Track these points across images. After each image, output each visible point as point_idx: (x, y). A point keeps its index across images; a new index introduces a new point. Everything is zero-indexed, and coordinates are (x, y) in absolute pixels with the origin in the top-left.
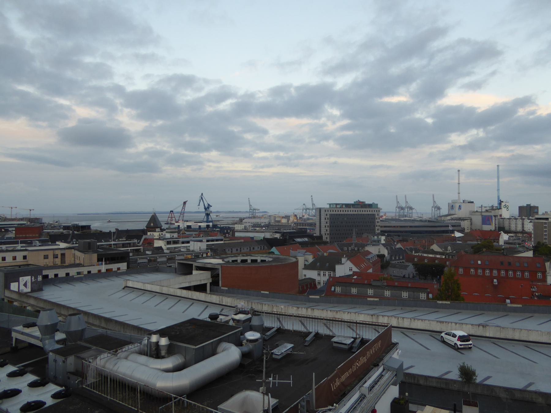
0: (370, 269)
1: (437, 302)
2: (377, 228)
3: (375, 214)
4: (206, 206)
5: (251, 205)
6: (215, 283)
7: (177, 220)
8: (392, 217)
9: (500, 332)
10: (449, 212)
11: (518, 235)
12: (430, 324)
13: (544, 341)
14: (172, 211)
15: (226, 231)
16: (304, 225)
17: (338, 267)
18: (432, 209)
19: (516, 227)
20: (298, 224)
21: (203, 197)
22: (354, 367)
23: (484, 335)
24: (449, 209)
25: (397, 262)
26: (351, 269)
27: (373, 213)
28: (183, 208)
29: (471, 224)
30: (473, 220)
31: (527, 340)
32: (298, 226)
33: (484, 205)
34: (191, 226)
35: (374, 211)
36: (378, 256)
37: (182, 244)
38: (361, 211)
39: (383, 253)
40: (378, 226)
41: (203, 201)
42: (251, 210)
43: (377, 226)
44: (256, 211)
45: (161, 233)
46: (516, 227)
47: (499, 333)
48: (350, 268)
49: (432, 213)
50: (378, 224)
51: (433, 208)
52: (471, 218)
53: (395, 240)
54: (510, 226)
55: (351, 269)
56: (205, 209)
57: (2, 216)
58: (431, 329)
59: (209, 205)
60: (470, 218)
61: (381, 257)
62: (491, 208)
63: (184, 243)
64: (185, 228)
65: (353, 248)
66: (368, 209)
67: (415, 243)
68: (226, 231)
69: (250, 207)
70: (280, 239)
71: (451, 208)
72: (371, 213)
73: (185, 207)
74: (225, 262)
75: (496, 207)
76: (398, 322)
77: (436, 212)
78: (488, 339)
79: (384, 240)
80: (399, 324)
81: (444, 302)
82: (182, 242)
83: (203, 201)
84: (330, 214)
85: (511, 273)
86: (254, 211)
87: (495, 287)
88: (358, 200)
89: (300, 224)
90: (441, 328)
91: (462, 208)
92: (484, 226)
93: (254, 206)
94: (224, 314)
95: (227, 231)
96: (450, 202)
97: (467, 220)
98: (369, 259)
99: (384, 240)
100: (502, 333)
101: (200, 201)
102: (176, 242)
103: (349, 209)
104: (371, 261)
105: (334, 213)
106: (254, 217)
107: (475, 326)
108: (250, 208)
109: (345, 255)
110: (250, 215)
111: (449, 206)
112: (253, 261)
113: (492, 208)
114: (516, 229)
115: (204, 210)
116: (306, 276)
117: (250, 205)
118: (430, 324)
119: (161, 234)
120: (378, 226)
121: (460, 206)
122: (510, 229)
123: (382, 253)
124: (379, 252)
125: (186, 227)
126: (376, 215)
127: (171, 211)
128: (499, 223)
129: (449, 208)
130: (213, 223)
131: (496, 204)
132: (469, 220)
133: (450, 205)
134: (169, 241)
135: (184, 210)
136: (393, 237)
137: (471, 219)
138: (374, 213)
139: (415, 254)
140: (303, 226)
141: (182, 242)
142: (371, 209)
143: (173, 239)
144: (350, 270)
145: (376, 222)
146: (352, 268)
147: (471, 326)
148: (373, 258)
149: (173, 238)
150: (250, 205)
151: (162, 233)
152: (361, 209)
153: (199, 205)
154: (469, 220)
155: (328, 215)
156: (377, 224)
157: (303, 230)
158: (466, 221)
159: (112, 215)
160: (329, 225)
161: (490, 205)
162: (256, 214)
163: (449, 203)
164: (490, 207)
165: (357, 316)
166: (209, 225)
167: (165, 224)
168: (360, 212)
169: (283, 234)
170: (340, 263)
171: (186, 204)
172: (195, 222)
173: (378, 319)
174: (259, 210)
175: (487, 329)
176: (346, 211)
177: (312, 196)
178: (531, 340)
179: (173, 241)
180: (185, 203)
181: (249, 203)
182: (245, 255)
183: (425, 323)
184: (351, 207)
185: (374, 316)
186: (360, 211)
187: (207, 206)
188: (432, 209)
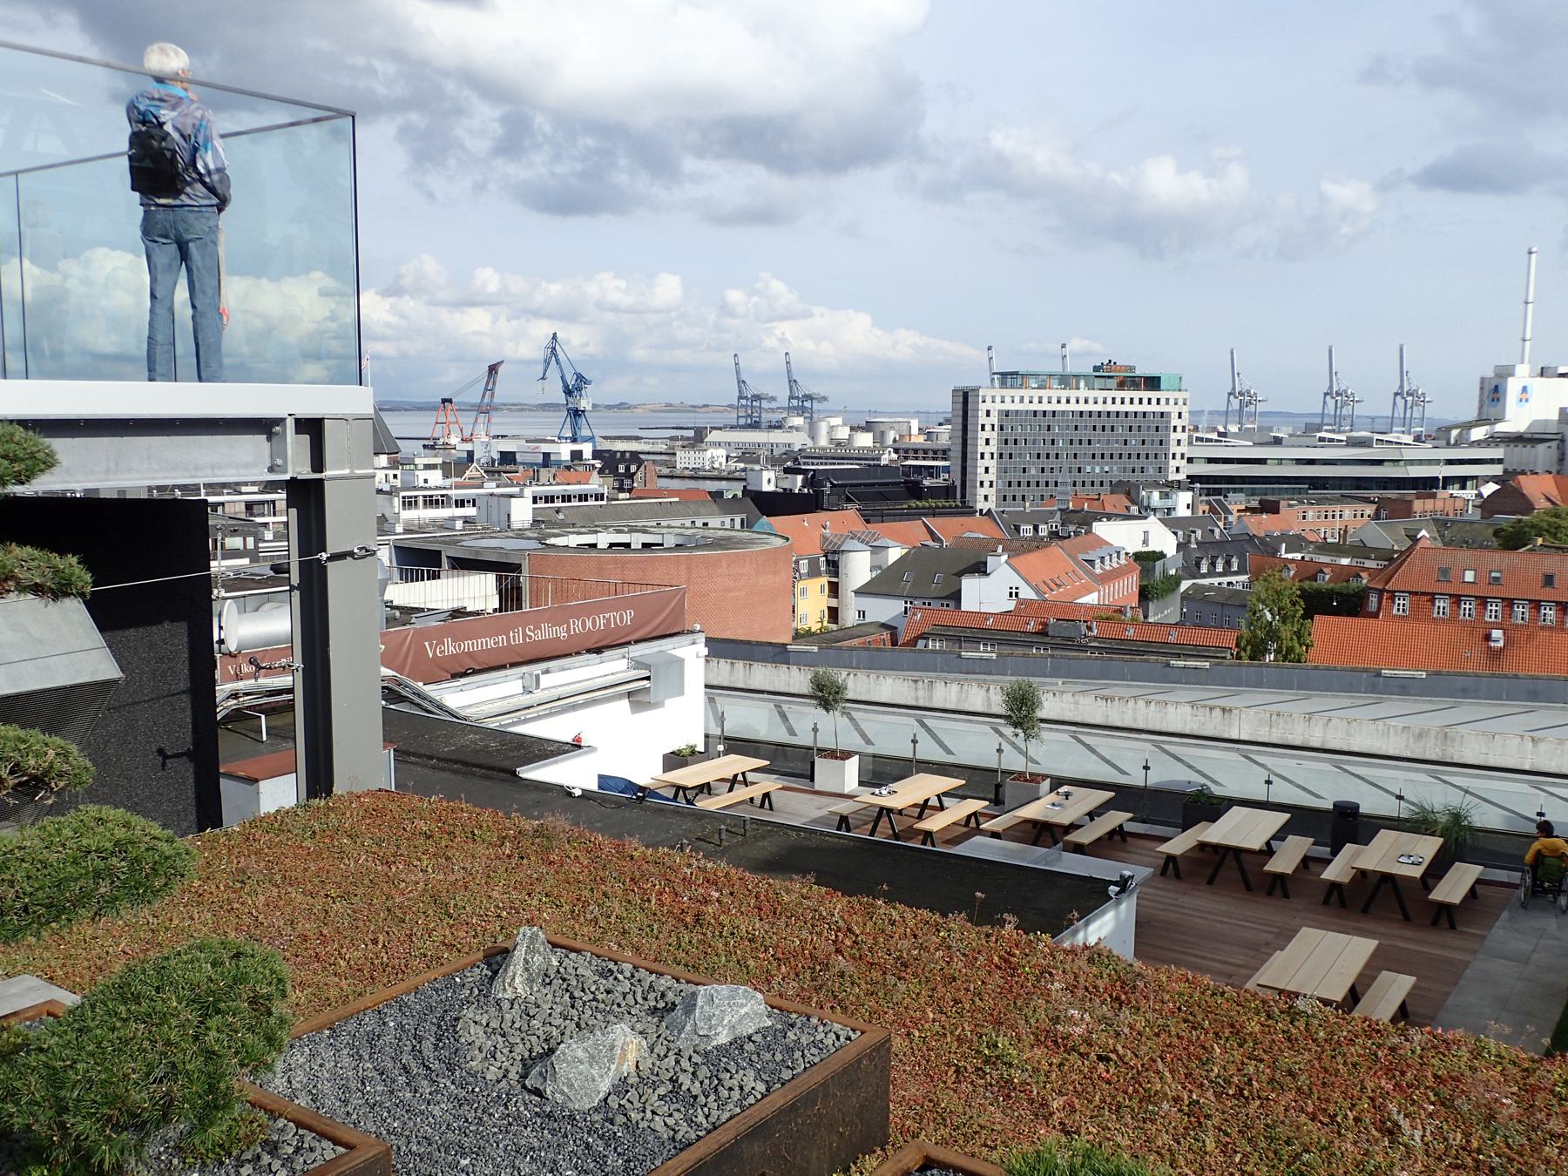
0: (1090, 593)
2: (1173, 464)
4: (571, 381)
5: (743, 382)
12: (1077, 703)
13: (1391, 752)
15: (622, 469)
18: (1395, 403)
21: (557, 347)
22: (514, 636)
23: (1226, 736)
26: (1014, 591)
27: (1163, 408)
31: (1346, 748)
32: (906, 458)
34: (514, 453)
37: (457, 506)
40: (1178, 456)
41: (557, 361)
42: (743, 402)
43: (1174, 458)
44: (765, 404)
45: (391, 473)
47: (1268, 729)
48: (1011, 588)
49: (1405, 418)
50: (1179, 450)
52: (1563, 436)
53: (1230, 507)
55: (1014, 591)
56: (568, 392)
58: (1078, 719)
59: (580, 377)
60: (1559, 437)
63: (463, 505)
65: (1056, 527)
66: (1145, 395)
67: (1304, 517)
68: (622, 469)
69: (739, 387)
71: (1492, 395)
72: (1154, 408)
76: (989, 699)
77: (1409, 411)
78: (1236, 746)
80: (989, 706)
82: (456, 501)
83: (557, 361)
84: (1000, 412)
86: (807, 404)
88: (1110, 361)
89: (916, 451)
90: (1108, 716)
93: (754, 388)
95: (628, 469)
96: (1490, 373)
97: (1548, 444)
99: (1188, 507)
100: (1274, 730)
103: (1073, 394)
104: (1098, 571)
106: (755, 426)
109: (1001, 547)
110: (738, 417)
111: (1482, 388)
115: (561, 398)
117: (741, 382)
119: (391, 477)
120: (1178, 456)
121: (1524, 389)
124: (1145, 542)
125: (496, 456)
127: (444, 401)
129: (1481, 395)
130: (594, 446)
136: (1226, 496)
137: (1562, 441)
138: (1004, 392)
139: (1290, 556)
142: (1154, 395)
145: (1173, 443)
146: (1017, 588)
147: (1190, 709)
148: (1107, 558)
149: (426, 485)
150: (741, 382)
151: (395, 472)
152: (1119, 394)
153: (543, 378)
154: (1554, 444)
155: (994, 414)
156: (1173, 449)
158: (1541, 447)
160: (994, 450)
166: (581, 452)
167: (425, 446)
169: (813, 480)
170: (980, 569)
171: (496, 373)
172: (527, 442)
174: (773, 399)
178: (1356, 749)
179: (425, 496)
181: (738, 373)
183: (1062, 701)
184: (1082, 384)
187: (573, 382)
188: (1395, 403)
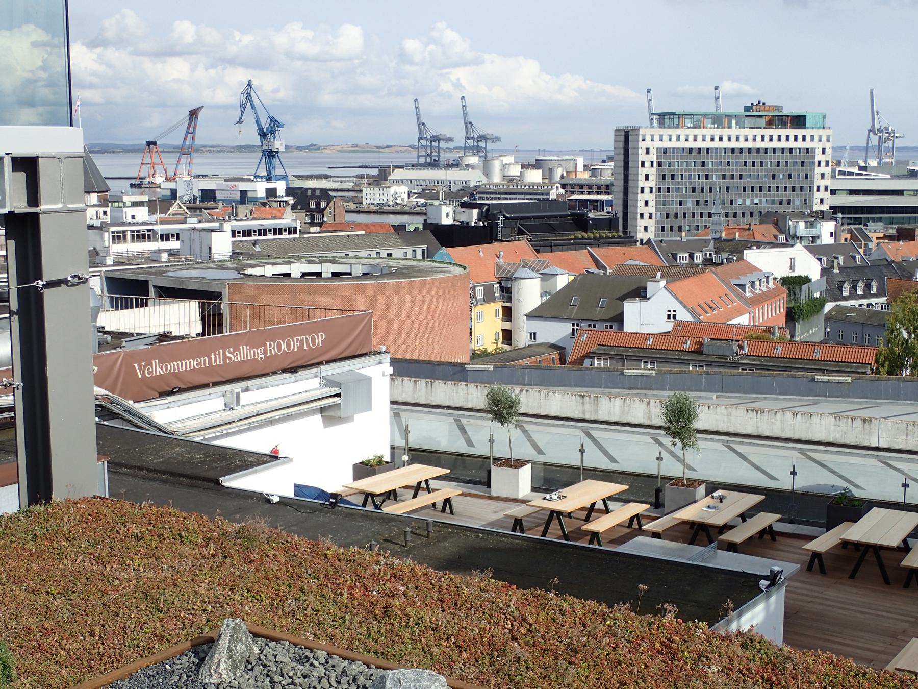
1: (816, 377)
2: (817, 196)
4: (265, 124)
9: (907, 436)
12: (729, 415)
15: (313, 205)
20: (573, 186)
21: (252, 93)
23: (866, 444)
25: (857, 303)
26: (672, 313)
27: (808, 144)
28: (187, 133)
32: (573, 193)
36: (786, 281)
38: (784, 138)
39: (803, 274)
40: (822, 189)
41: (253, 107)
42: (423, 142)
43: (818, 190)
44: (443, 145)
45: (101, 210)
47: (904, 437)
48: (669, 311)
50: (822, 183)
53: (870, 235)
55: (672, 313)
56: (263, 135)
59: (273, 121)
63: (167, 239)
64: (195, 198)
65: (710, 254)
66: (792, 132)
73: (195, 127)
74: (762, 497)
76: (649, 412)
79: (831, 234)
80: (650, 418)
81: (834, 378)
82: (162, 235)
83: (253, 107)
86: (482, 144)
88: (759, 102)
89: (581, 186)
93: (433, 129)
95: (318, 204)
98: (742, 287)
100: (910, 438)
102: (144, 235)
103: (725, 132)
104: (749, 294)
105: (674, 146)
106: (434, 164)
107: (845, 420)
108: (420, 133)
110: (419, 157)
116: (535, 339)
117: (421, 125)
118: (729, 415)
119: (102, 213)
120: (822, 189)
123: (799, 272)
124: (792, 268)
125: (198, 194)
126: (819, 151)
130: (287, 184)
134: (119, 232)
135: (193, 138)
136: (866, 225)
141: (162, 235)
142: (800, 132)
143: (133, 224)
145: (817, 176)
146: (674, 311)
148: (757, 283)
149: (134, 221)
150: (468, 124)
153: (239, 122)
155: (653, 152)
156: (818, 182)
159: (554, 468)
162: (442, 155)
165: (543, 396)
168: (763, 140)
169: (487, 214)
170: (640, 293)
171: (197, 117)
172: (226, 180)
173: (597, 404)
175: (872, 426)
176: (788, 138)
177: (416, 100)
179: (132, 231)
181: (418, 115)
182: (317, 260)
183: (716, 414)
184: (734, 123)
185: (587, 398)
186: (763, 137)
187: (267, 125)
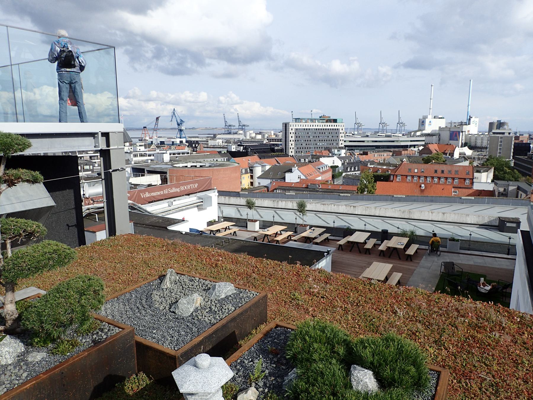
2: (340, 142)
3: (339, 129)
4: (179, 122)
6: (164, 180)
7: (151, 137)
8: (54, 154)
10: (419, 128)
11: (482, 151)
12: (316, 206)
14: (146, 127)
15: (194, 145)
16: (279, 141)
17: (288, 175)
18: (397, 126)
19: (482, 142)
21: (175, 112)
24: (419, 125)
26: (299, 177)
29: (439, 140)
30: (441, 135)
31: (385, 216)
32: (270, 142)
33: (453, 121)
35: (339, 125)
41: (175, 116)
42: (226, 127)
44: (232, 127)
45: (130, 147)
46: (482, 142)
50: (342, 139)
51: (398, 124)
53: (355, 154)
54: (476, 142)
55: (299, 177)
57: (2, 131)
59: (181, 120)
61: (334, 168)
62: (460, 124)
63: (150, 156)
64: (158, 144)
66: (333, 124)
70: (242, 152)
73: (158, 122)
75: (465, 123)
76: (293, 205)
77: (401, 128)
83: (175, 116)
85: (409, 178)
87: (422, 191)
89: (273, 140)
91: (432, 123)
92: (451, 141)
94: (260, 213)
96: (421, 118)
97: (436, 136)
98: (319, 169)
101: (172, 117)
103: (314, 124)
104: (321, 171)
106: (230, 133)
108: (225, 124)
111: (419, 122)
112: (355, 174)
113: (462, 124)
114: (482, 145)
115: (177, 126)
118: (316, 206)
119: (130, 149)
122: (476, 144)
124: (333, 163)
125: (159, 142)
127: (144, 127)
128: (466, 139)
131: (465, 120)
132: (437, 136)
133: (420, 121)
135: (158, 126)
137: (440, 135)
139: (371, 166)
140: (278, 142)
142: (335, 124)
144: (298, 177)
145: (340, 137)
151: (131, 147)
152: (326, 124)
153: (171, 121)
154: (437, 136)
156: (341, 138)
157: (70, 154)
158: (434, 137)
160: (294, 139)
161: (460, 121)
163: (420, 119)
164: (459, 123)
167: (139, 140)
169: (245, 148)
170: (290, 171)
180: (157, 119)
188: (397, 126)
